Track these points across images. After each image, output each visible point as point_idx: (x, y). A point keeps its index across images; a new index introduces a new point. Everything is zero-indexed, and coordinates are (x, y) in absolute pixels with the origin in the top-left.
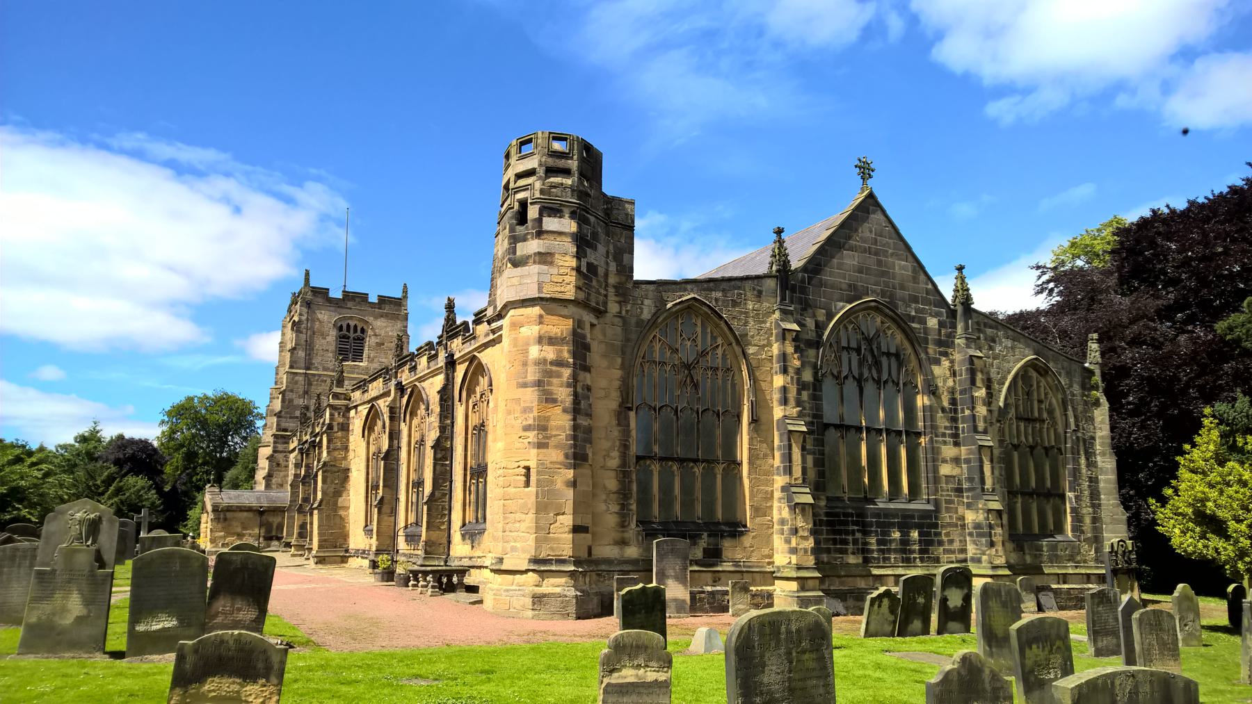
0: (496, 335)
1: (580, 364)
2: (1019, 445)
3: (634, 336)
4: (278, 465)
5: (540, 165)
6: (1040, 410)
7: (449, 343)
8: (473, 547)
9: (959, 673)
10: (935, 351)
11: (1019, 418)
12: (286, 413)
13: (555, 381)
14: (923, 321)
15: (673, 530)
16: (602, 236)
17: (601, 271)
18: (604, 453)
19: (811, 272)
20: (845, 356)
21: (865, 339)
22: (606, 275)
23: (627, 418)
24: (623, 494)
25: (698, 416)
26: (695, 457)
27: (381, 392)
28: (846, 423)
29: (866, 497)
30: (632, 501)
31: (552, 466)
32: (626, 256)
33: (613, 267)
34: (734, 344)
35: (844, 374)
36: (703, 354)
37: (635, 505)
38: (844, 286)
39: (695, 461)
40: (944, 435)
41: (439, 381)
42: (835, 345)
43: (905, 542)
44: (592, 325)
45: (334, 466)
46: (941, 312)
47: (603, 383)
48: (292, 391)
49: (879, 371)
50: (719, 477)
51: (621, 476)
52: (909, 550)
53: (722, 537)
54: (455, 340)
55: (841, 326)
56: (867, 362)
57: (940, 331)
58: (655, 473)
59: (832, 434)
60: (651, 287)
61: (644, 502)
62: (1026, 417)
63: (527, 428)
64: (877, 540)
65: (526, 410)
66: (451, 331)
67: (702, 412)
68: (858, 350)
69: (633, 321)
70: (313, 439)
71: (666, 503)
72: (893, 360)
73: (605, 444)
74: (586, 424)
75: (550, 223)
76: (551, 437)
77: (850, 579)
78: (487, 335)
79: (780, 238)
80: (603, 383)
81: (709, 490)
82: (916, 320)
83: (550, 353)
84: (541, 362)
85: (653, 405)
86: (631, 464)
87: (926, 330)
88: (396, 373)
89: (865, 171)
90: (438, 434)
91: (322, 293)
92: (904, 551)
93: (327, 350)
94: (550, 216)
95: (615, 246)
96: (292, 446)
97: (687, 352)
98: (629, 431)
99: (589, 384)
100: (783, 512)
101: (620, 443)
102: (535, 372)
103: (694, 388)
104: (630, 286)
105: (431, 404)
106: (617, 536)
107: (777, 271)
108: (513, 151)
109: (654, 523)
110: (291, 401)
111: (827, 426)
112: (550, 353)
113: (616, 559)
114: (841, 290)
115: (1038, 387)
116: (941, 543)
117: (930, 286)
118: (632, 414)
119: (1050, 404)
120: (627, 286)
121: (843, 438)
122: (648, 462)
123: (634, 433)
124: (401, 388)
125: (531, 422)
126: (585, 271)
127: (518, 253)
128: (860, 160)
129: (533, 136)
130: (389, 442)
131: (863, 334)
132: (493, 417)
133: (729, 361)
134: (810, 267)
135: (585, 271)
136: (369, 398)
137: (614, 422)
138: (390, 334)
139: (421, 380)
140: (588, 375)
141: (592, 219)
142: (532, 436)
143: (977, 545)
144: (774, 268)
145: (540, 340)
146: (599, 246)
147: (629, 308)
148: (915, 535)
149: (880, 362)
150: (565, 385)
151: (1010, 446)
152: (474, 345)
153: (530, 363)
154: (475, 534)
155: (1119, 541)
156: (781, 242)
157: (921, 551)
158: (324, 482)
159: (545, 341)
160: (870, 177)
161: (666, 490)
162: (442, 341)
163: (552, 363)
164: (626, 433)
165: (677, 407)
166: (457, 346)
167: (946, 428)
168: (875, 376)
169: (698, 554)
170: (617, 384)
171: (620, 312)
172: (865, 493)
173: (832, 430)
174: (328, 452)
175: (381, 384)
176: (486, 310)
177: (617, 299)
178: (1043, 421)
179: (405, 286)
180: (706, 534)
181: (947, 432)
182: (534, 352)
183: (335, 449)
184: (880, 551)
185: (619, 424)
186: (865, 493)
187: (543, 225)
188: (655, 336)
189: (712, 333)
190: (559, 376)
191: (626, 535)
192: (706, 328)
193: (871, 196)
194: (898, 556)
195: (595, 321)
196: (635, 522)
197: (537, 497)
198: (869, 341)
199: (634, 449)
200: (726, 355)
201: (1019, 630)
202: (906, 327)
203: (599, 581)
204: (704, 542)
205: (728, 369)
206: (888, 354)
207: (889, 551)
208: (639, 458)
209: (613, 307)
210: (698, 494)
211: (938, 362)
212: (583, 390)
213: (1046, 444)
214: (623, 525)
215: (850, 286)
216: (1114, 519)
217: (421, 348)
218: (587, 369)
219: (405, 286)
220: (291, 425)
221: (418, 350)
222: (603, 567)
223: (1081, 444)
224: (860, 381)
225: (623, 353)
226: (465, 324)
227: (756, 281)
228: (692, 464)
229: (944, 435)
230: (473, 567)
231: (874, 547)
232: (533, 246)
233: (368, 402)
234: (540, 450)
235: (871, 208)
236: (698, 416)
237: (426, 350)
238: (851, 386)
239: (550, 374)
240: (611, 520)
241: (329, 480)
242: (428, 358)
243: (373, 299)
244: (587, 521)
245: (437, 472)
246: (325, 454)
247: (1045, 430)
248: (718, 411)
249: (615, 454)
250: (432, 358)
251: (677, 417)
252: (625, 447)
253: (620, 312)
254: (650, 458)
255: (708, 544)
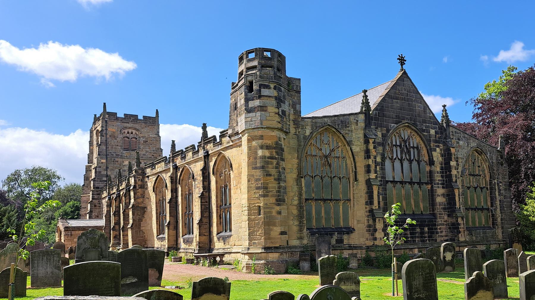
0: (234, 143)
1: (281, 158)
2: (470, 187)
3: (302, 144)
4: (95, 206)
5: (259, 64)
6: (479, 170)
7: (205, 146)
8: (224, 243)
9: (476, 279)
10: (434, 145)
11: (470, 175)
12: (98, 179)
13: (270, 166)
14: (429, 132)
15: (322, 232)
16: (287, 97)
17: (287, 113)
18: (292, 198)
19: (380, 110)
20: (394, 148)
21: (403, 141)
22: (289, 115)
23: (301, 182)
24: (300, 217)
25: (331, 179)
26: (330, 198)
27: (164, 169)
28: (396, 180)
29: (405, 213)
30: (304, 219)
31: (270, 205)
32: (298, 106)
33: (292, 112)
34: (346, 146)
35: (394, 157)
36: (333, 150)
37: (305, 221)
38: (394, 116)
39: (331, 200)
40: (438, 184)
41: (200, 165)
42: (390, 144)
43: (422, 233)
44: (284, 139)
45: (138, 206)
46: (436, 127)
47: (290, 166)
48: (100, 167)
49: (410, 155)
50: (341, 207)
51: (299, 208)
52: (424, 236)
53: (344, 234)
54: (209, 145)
55: (393, 135)
56: (404, 151)
57: (436, 136)
58: (313, 206)
59: (390, 185)
60: (309, 120)
61: (309, 220)
62: (473, 174)
63: (258, 188)
64: (410, 232)
65: (257, 180)
66: (206, 140)
67: (333, 178)
68: (400, 146)
69: (302, 137)
70: (118, 192)
71: (318, 219)
72: (416, 150)
73: (292, 194)
74: (284, 185)
75: (265, 92)
76: (269, 192)
77: (399, 250)
78: (229, 142)
79: (366, 94)
80: (290, 166)
81: (337, 213)
82: (425, 131)
83: (267, 153)
84: (263, 157)
85: (311, 175)
86: (303, 203)
87: (430, 136)
88: (173, 160)
89: (402, 61)
90: (202, 191)
91: (113, 115)
92: (422, 237)
93: (118, 145)
94: (264, 88)
95: (293, 102)
96: (103, 196)
97: (326, 150)
98: (302, 188)
99: (284, 167)
100: (370, 222)
101: (298, 193)
102: (261, 162)
103: (329, 167)
104: (299, 120)
105: (195, 176)
106: (298, 235)
107: (365, 111)
108: (244, 57)
109: (314, 229)
110: (100, 172)
111: (387, 182)
112: (267, 153)
113: (298, 246)
114: (392, 118)
115: (478, 160)
116: (437, 233)
117: (431, 115)
118: (303, 180)
119: (483, 168)
120: (299, 121)
121: (394, 187)
122: (310, 201)
123: (304, 188)
124: (176, 168)
125: (260, 185)
126: (281, 114)
127: (250, 106)
128: (399, 56)
129: (254, 50)
130: (171, 194)
131: (402, 138)
132: (233, 182)
133: (344, 153)
134: (379, 108)
135: (281, 114)
136: (156, 172)
137: (295, 184)
138: (151, 136)
139: (189, 163)
140: (283, 162)
141: (282, 89)
142: (261, 192)
143: (453, 233)
144: (364, 109)
145: (262, 147)
146: (286, 102)
147: (300, 131)
148: (426, 229)
149: (410, 151)
150: (274, 167)
151: (466, 187)
152: (220, 147)
153: (258, 158)
154: (226, 238)
155: (515, 229)
156: (366, 96)
157: (429, 237)
158: (133, 214)
159: (265, 147)
160: (405, 64)
161: (318, 213)
162: (201, 145)
163: (269, 158)
164: (300, 188)
165: (322, 176)
166: (210, 147)
167: (439, 180)
168: (408, 158)
169: (333, 241)
170: (296, 166)
171: (296, 133)
172: (405, 211)
173: (389, 183)
174: (135, 200)
175: (163, 165)
176: (227, 130)
177: (295, 126)
178: (480, 175)
179: (157, 110)
180: (336, 233)
181: (440, 182)
182: (260, 153)
183: (138, 198)
184: (411, 237)
185: (297, 185)
186: (405, 211)
187: (262, 92)
188: (311, 143)
189: (336, 141)
190: (272, 164)
191: (302, 235)
192: (334, 139)
193: (405, 73)
194: (419, 239)
195: (285, 137)
196: (306, 229)
197: (264, 219)
198: (405, 141)
199: (304, 196)
200: (343, 151)
201: (486, 266)
202: (421, 134)
203: (291, 256)
204: (336, 236)
205: (344, 157)
206: (413, 147)
207: (415, 237)
208: (306, 200)
209: (292, 130)
210: (332, 215)
211: (435, 150)
212: (282, 169)
213: (482, 186)
214: (301, 230)
215: (396, 116)
216: (510, 219)
217: (188, 148)
218: (283, 160)
219: (157, 110)
220: (101, 185)
221: (186, 149)
222: (293, 250)
223: (496, 185)
224: (401, 160)
225: (298, 152)
226: (214, 137)
227: (355, 115)
228: (329, 202)
229: (438, 184)
230: (227, 253)
231: (409, 236)
232: (256, 103)
233: (156, 174)
234: (265, 198)
235: (405, 79)
236: (331, 179)
237: (191, 149)
238: (397, 164)
239: (268, 163)
240: (295, 229)
241: (136, 213)
242: (192, 153)
243: (140, 117)
244: (286, 229)
245: (202, 209)
246: (132, 201)
247: (481, 179)
248: (340, 177)
249: (296, 198)
250: (196, 153)
251: (322, 180)
252: (300, 194)
253: (296, 133)
254: (311, 199)
255: (338, 238)
